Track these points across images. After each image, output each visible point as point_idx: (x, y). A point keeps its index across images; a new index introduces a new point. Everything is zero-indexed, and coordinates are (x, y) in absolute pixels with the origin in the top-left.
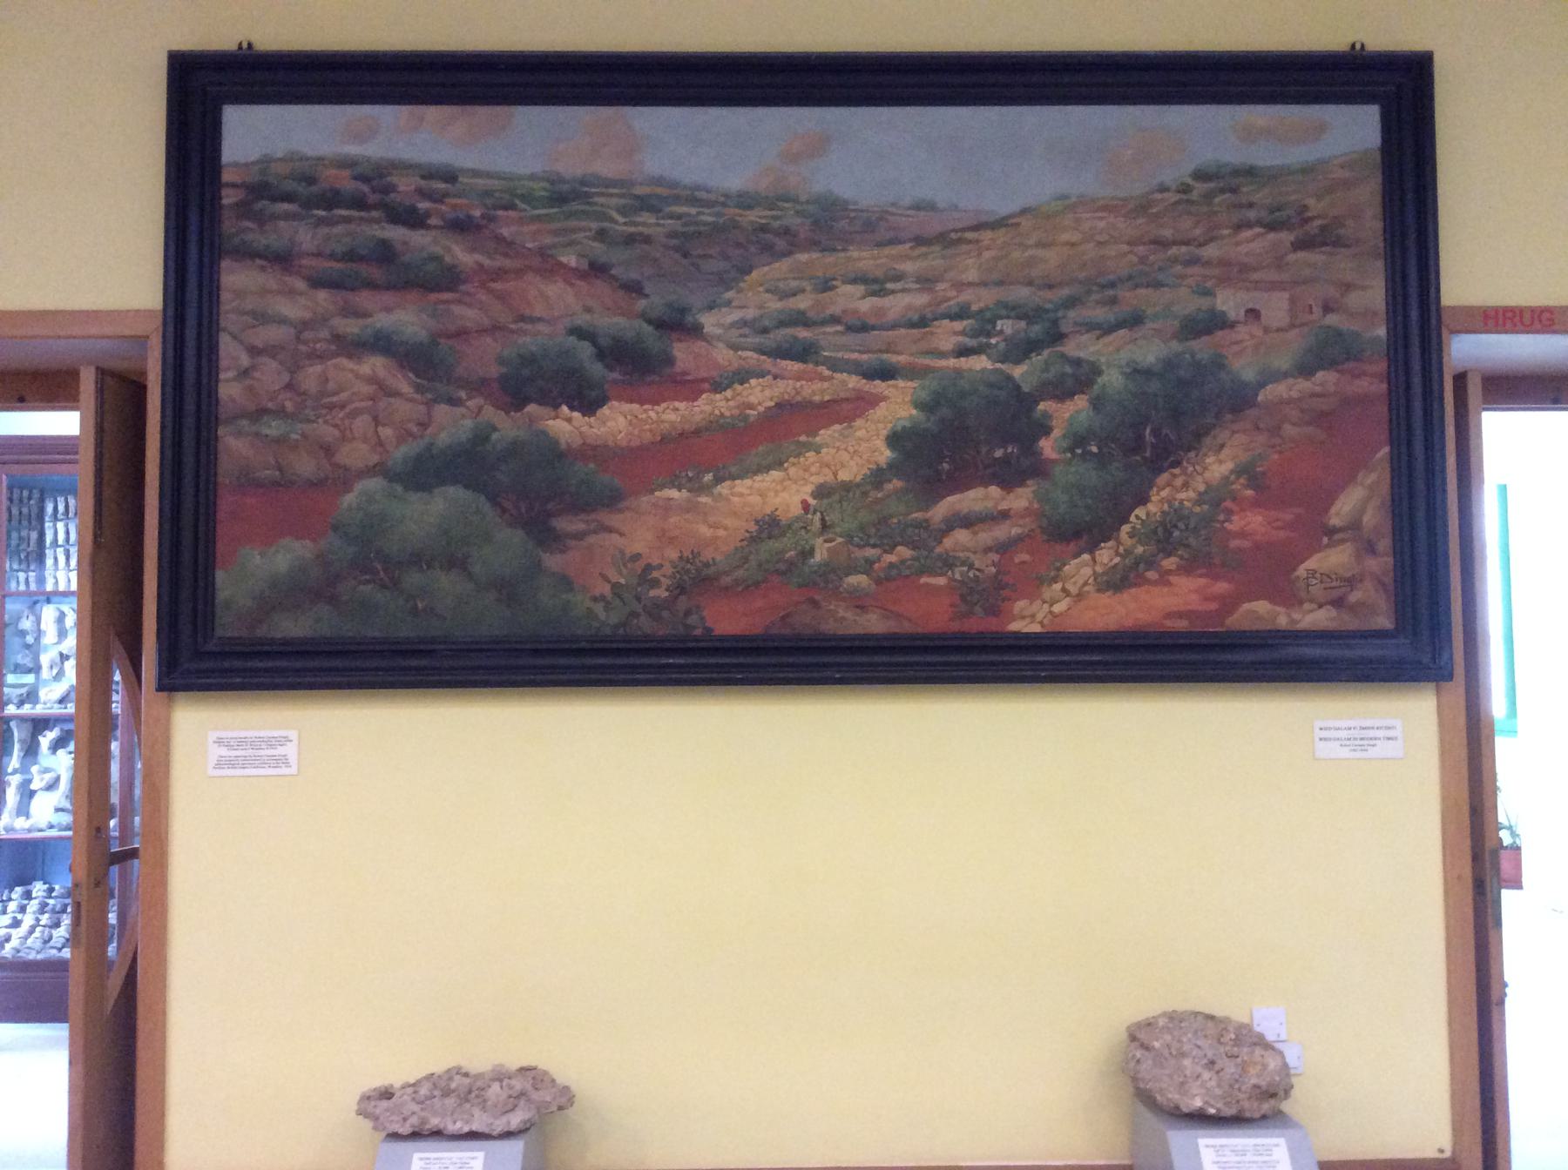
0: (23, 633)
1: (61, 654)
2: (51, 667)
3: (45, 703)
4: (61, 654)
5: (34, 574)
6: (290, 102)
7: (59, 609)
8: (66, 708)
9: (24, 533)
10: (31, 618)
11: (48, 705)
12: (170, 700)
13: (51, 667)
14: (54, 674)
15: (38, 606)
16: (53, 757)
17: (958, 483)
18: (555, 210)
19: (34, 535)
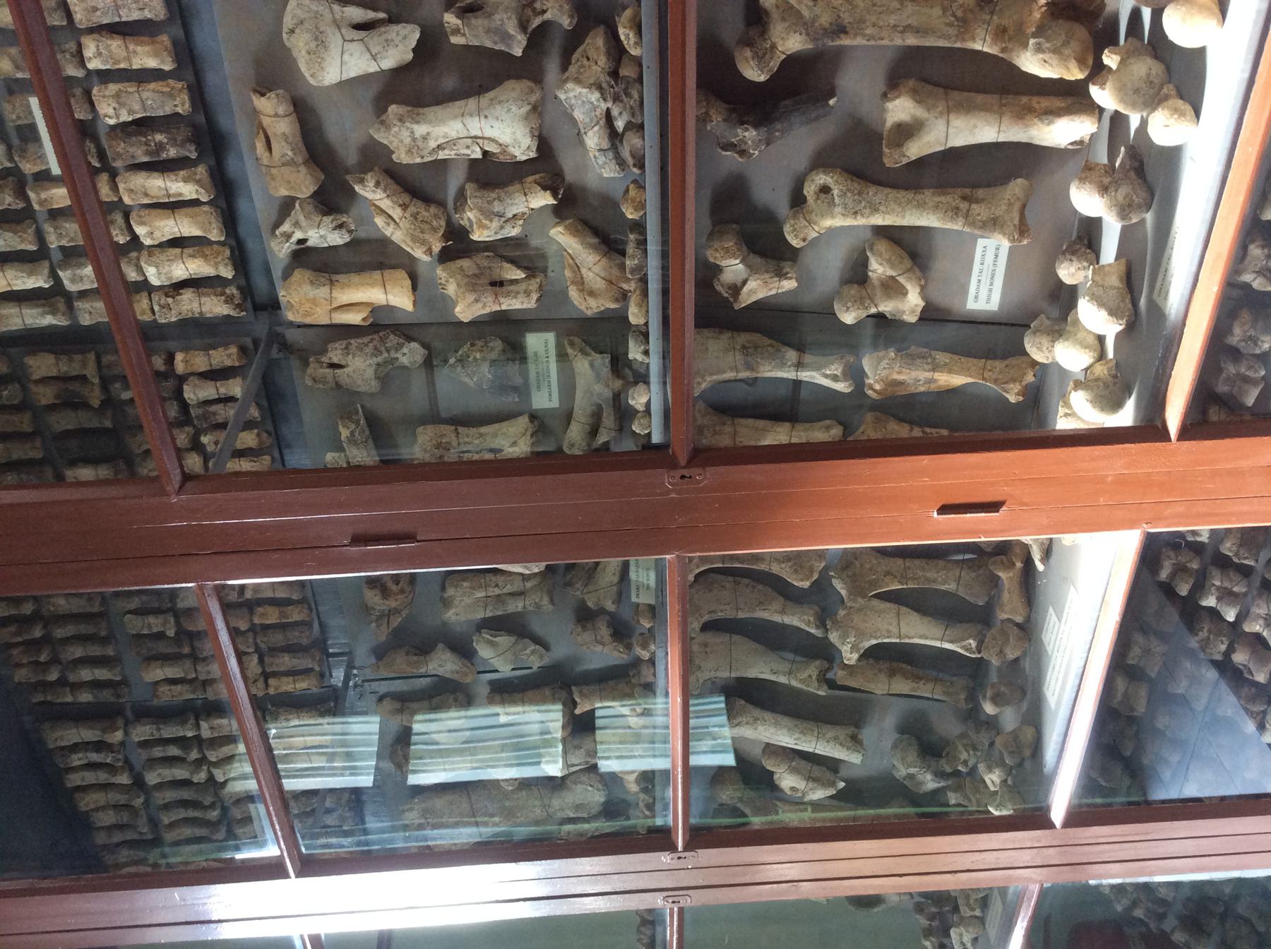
0: (388, 376)
1: (445, 256)
2: (498, 284)
3: (624, 296)
4: (445, 256)
5: (179, 357)
6: (1094, 445)
7: (287, 275)
8: (639, 227)
9: (45, 395)
10: (335, 355)
11: (630, 286)
12: (1053, 342)
13: (498, 284)
14: (519, 274)
15: (292, 335)
16: (807, 259)
17: (1126, 152)
18: (1246, 562)
19: (42, 365)
